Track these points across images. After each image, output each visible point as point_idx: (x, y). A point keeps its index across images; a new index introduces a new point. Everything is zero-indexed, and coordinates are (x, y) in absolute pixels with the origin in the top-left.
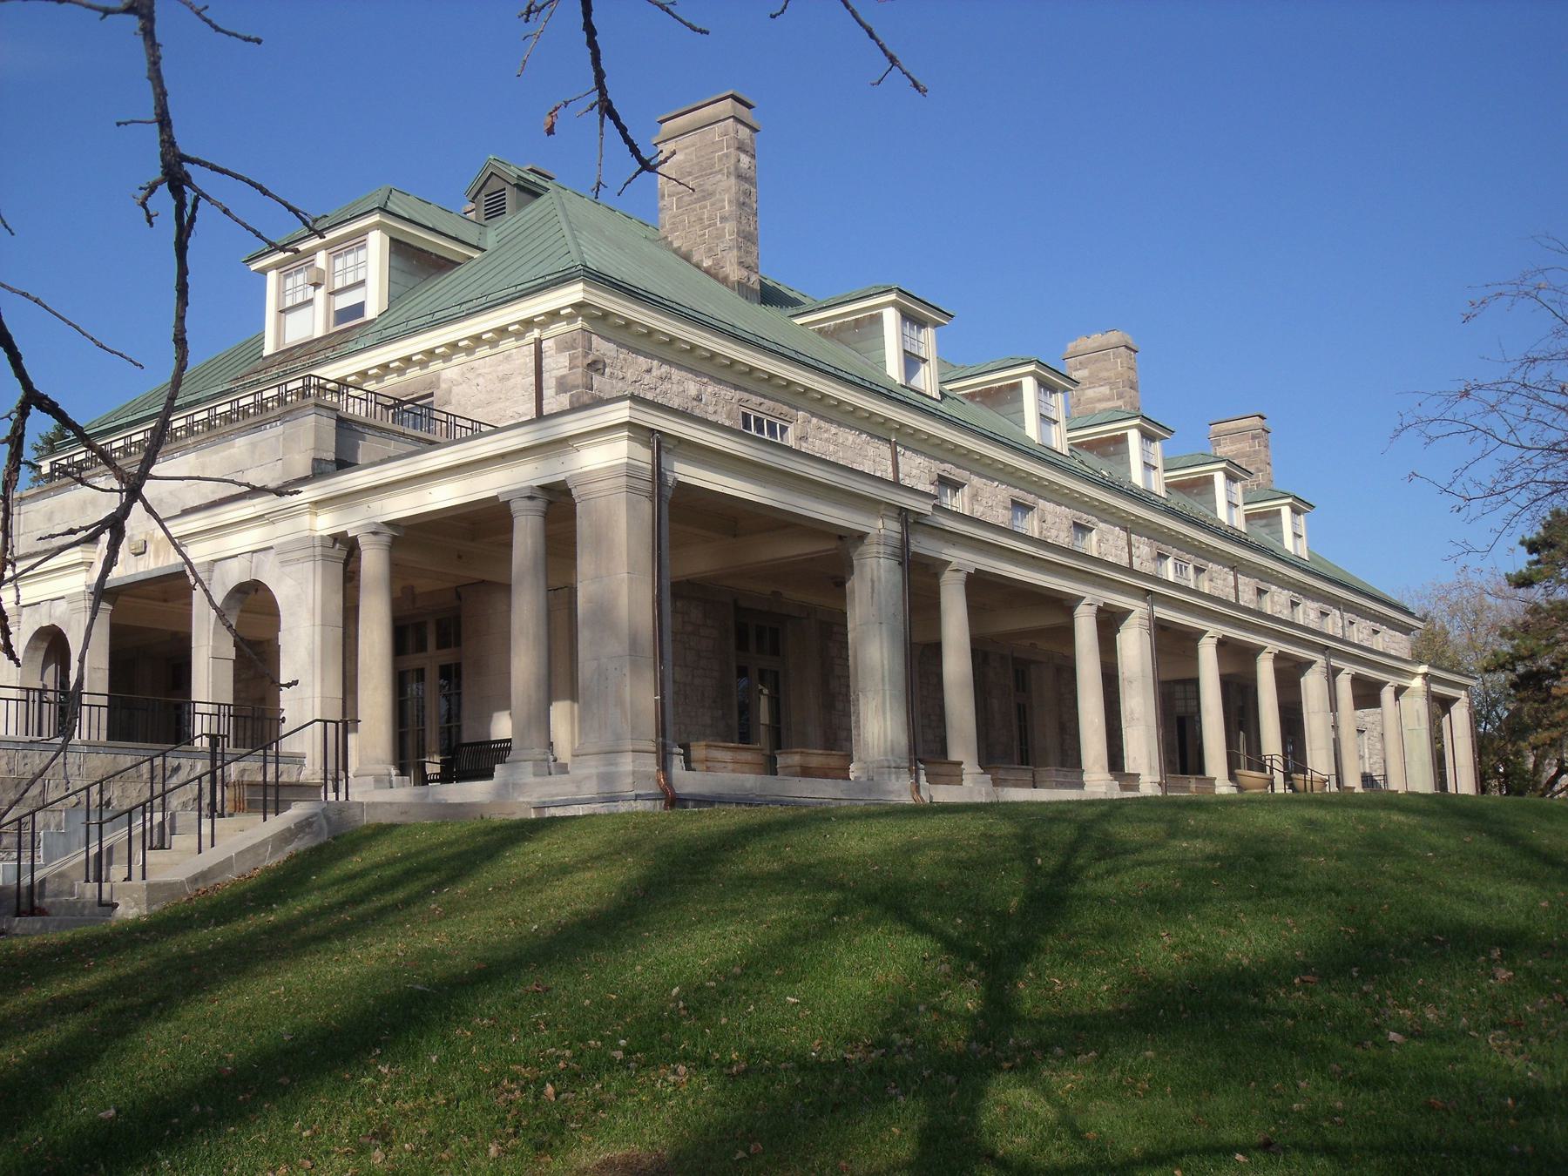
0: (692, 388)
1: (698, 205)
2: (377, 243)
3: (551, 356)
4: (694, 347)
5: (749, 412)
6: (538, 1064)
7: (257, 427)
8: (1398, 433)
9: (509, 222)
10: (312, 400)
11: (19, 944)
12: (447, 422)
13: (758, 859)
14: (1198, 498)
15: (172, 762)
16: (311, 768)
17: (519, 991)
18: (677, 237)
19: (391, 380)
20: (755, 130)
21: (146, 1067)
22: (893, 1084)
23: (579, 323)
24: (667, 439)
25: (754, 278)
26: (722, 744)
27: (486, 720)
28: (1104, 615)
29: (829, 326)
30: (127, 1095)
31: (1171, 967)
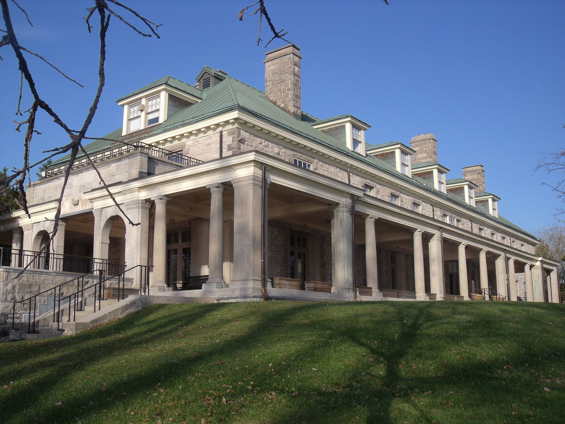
0: (276, 150)
2: (164, 96)
3: (226, 137)
4: (277, 135)
5: (296, 159)
6: (219, 390)
7: (119, 160)
8: (537, 168)
11: (29, 343)
12: (188, 160)
13: (300, 319)
14: (458, 195)
15: (86, 280)
16: (135, 283)
18: (271, 96)
20: (300, 58)
21: (74, 387)
22: (354, 401)
23: (236, 125)
24: (269, 167)
25: (299, 111)
26: (285, 278)
27: (199, 268)
28: (425, 236)
29: (326, 129)
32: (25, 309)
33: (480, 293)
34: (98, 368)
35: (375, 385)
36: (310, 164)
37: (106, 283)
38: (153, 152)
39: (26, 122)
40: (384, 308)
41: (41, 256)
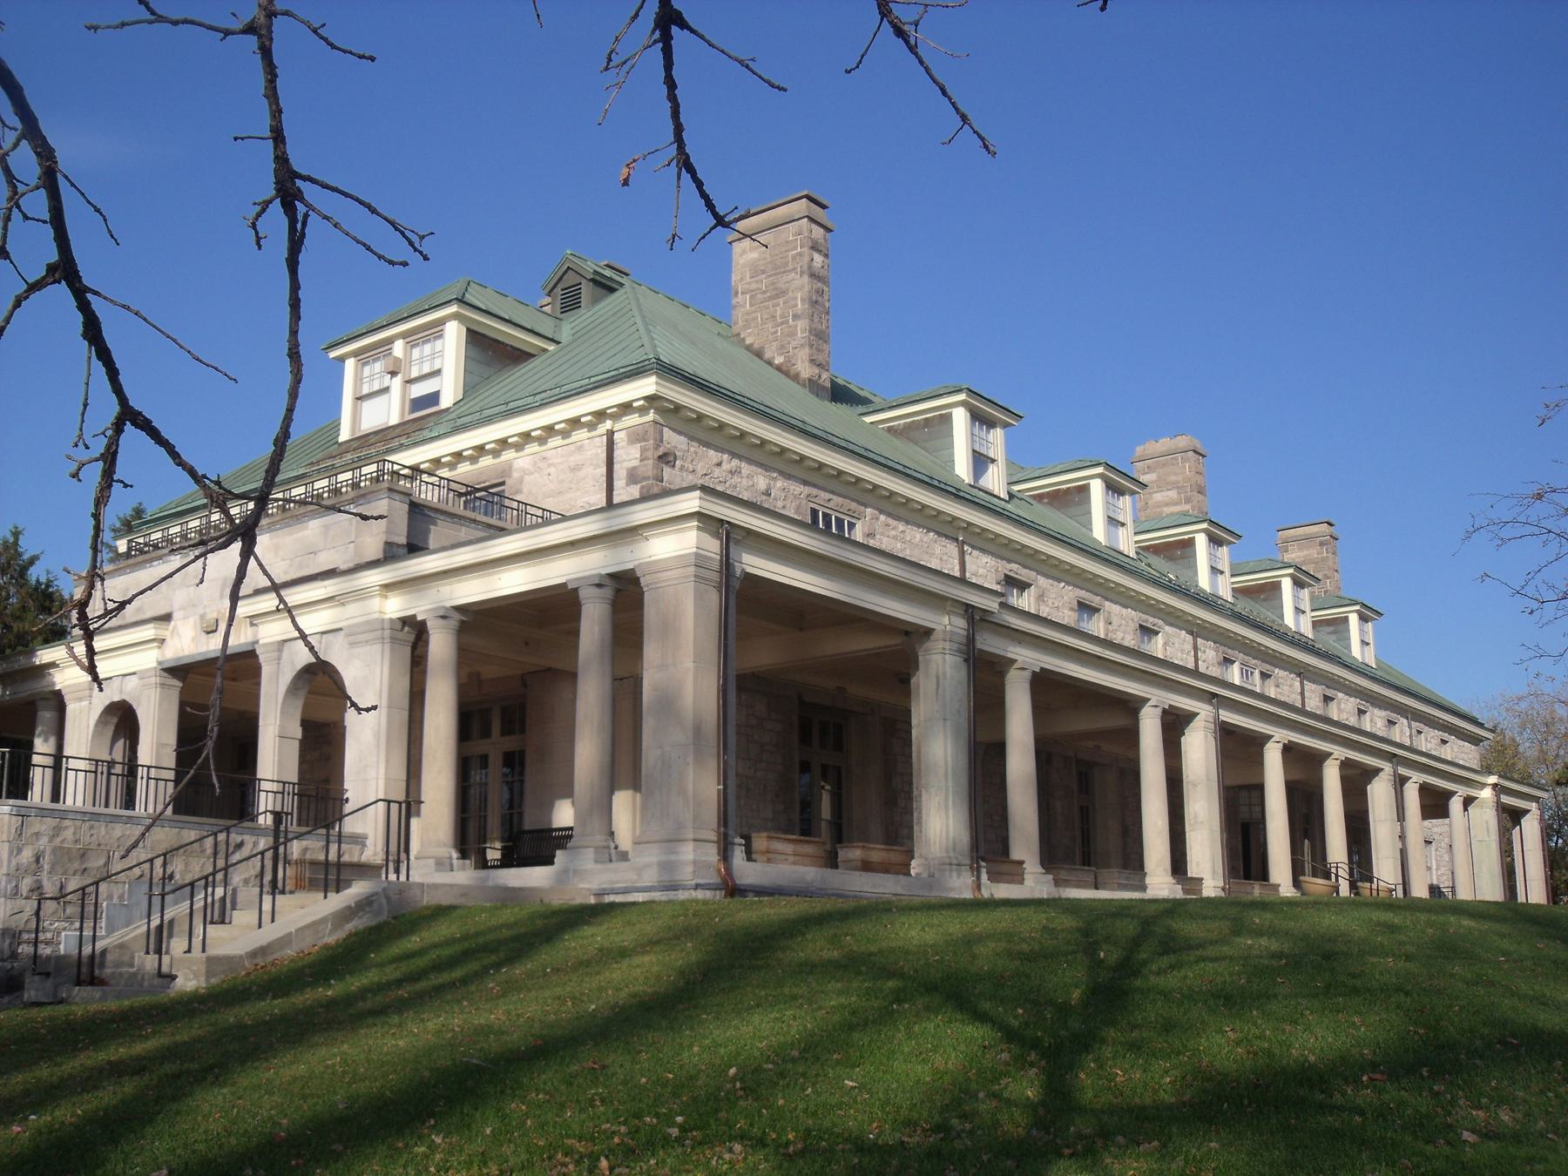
0: (762, 482)
1: (770, 303)
2: (454, 333)
3: (623, 448)
4: (764, 442)
5: (817, 507)
6: (593, 1139)
8: (1469, 535)
9: (585, 316)
10: (385, 485)
11: (78, 1010)
13: (817, 946)
14: (1264, 604)
15: (236, 838)
17: (575, 1068)
18: (750, 334)
19: (464, 469)
20: (828, 230)
21: (200, 1131)
23: (651, 416)
25: (825, 376)
26: (783, 836)
27: (548, 808)
30: (179, 1156)
31: (1235, 1061)
32: (68, 919)
33: (1327, 875)
34: (267, 1080)
35: (1010, 1126)
36: (854, 521)
37: (292, 847)
38: (423, 488)
39: (97, 460)
40: (1047, 919)
41: (113, 771)
